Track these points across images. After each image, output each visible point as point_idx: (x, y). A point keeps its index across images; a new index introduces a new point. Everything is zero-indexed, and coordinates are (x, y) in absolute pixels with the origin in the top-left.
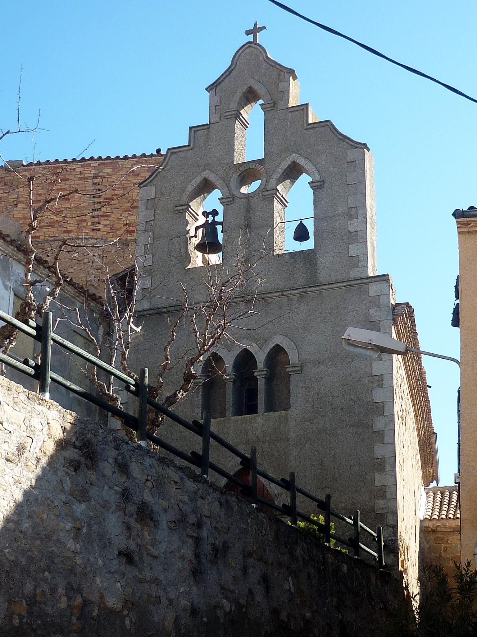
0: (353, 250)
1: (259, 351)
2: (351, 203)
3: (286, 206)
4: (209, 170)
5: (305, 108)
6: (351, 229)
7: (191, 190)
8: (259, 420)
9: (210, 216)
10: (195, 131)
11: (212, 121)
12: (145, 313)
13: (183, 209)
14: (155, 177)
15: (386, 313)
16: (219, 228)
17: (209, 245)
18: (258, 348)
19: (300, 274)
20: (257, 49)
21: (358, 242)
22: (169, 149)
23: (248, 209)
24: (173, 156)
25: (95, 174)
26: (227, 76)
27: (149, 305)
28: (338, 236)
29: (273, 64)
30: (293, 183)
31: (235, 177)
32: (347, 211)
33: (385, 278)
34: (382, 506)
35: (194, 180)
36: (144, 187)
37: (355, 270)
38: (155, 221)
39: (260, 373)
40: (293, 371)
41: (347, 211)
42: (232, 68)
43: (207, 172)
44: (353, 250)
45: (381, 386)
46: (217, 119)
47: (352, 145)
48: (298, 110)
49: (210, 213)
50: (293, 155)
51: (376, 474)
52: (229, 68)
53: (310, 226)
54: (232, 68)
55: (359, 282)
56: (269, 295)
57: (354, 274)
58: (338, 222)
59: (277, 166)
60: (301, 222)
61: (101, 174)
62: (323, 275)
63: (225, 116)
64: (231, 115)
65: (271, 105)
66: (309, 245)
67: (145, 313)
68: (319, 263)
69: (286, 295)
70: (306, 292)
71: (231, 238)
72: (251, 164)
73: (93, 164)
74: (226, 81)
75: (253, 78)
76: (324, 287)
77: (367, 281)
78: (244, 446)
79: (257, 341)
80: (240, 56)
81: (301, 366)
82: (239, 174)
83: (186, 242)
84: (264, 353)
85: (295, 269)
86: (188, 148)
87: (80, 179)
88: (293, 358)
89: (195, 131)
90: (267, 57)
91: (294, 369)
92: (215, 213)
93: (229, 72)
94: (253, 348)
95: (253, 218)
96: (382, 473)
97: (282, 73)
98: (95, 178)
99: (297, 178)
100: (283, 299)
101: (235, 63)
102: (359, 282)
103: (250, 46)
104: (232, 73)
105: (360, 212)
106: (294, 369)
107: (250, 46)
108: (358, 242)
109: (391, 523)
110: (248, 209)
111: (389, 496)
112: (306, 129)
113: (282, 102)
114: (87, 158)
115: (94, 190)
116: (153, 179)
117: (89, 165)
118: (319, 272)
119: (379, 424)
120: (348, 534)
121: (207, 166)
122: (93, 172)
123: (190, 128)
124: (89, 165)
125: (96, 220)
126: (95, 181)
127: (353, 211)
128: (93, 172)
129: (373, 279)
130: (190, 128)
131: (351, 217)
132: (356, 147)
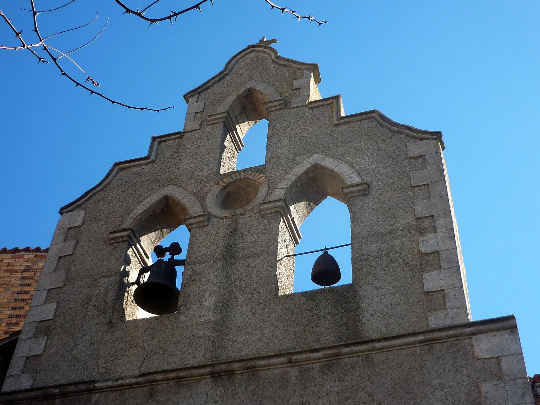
0: (432, 281)
2: (421, 210)
3: (297, 243)
5: (335, 104)
6: (424, 250)
7: (140, 211)
9: (167, 254)
10: (160, 142)
11: (187, 130)
12: (21, 396)
14: (88, 200)
16: (180, 269)
19: (326, 326)
21: (440, 268)
22: (117, 164)
24: (122, 173)
25: (28, 266)
26: (217, 82)
27: (31, 381)
28: (400, 261)
29: (285, 63)
30: (310, 209)
32: (414, 223)
33: (506, 325)
35: (148, 199)
37: (440, 314)
38: (74, 256)
41: (414, 223)
44: (432, 281)
46: (196, 125)
48: (323, 105)
49: (167, 249)
50: (314, 156)
52: (222, 72)
56: (262, 362)
57: (437, 320)
58: (399, 241)
60: (326, 252)
61: (35, 267)
62: (373, 324)
63: (209, 121)
64: (218, 119)
65: (281, 102)
67: (21, 396)
68: (363, 305)
69: (297, 361)
70: (338, 355)
71: (200, 274)
73: (27, 255)
74: (215, 87)
76: (378, 345)
77: (468, 330)
82: (222, 187)
83: (123, 287)
85: (315, 317)
86: (145, 161)
87: (6, 271)
90: (278, 57)
98: (25, 271)
99: (317, 203)
100: (289, 369)
102: (452, 332)
104: (224, 79)
105: (440, 223)
107: (253, 51)
108: (440, 268)
112: (336, 125)
114: (21, 247)
115: (21, 285)
116: (85, 202)
117: (22, 257)
118: (364, 320)
121: (171, 181)
122: (25, 264)
124: (22, 257)
125: (14, 320)
126: (25, 274)
127: (427, 223)
128: (25, 264)
131: (422, 231)
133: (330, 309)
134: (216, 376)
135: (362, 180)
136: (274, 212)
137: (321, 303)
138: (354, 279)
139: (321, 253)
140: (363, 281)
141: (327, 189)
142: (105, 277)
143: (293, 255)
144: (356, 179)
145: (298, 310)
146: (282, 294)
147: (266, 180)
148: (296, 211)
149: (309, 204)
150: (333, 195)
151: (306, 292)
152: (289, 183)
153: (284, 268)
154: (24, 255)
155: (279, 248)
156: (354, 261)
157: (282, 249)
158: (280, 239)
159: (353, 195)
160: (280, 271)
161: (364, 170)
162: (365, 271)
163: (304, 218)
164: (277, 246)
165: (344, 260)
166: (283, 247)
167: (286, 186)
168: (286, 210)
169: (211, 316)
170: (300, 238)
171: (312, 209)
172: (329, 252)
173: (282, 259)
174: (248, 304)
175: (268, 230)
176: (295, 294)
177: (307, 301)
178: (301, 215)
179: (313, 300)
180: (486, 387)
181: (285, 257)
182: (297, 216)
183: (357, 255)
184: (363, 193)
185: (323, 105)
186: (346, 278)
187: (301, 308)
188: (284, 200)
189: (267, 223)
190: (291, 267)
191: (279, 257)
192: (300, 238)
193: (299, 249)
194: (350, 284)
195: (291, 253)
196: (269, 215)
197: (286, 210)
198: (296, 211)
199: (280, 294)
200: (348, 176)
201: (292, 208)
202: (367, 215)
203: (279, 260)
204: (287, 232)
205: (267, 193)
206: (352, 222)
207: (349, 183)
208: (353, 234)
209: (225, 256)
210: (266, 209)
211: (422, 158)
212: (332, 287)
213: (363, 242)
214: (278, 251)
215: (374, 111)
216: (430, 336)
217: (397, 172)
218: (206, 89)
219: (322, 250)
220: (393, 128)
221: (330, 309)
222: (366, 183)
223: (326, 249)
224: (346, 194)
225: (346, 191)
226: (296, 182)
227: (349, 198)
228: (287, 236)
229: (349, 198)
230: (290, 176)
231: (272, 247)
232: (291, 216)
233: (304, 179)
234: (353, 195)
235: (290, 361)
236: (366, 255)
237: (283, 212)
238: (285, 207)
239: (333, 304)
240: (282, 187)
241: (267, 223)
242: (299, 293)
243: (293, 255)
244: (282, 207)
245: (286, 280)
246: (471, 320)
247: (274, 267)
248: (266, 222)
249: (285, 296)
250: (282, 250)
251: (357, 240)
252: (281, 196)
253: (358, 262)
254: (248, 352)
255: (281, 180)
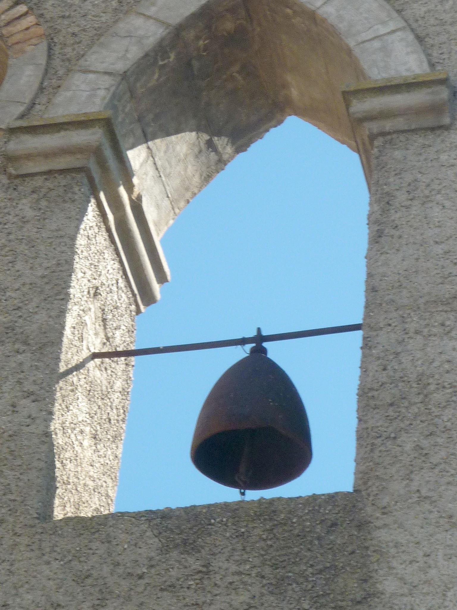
3: (148, 297)
60: (259, 352)
68: (389, 585)
99: (243, 136)
133: (256, 590)
135: (432, 65)
136: (62, 172)
137: (219, 563)
138: (364, 475)
139: (240, 353)
140: (397, 487)
141: (285, 86)
143: (128, 354)
144: (408, 61)
145: (125, 584)
146: (70, 511)
147: (40, 30)
148: (156, 168)
149: (210, 144)
150: (311, 113)
151: (165, 515)
152: (135, 53)
153: (83, 404)
154: (204, 42)
155: (70, 321)
156: (367, 397)
157: (83, 324)
158: (79, 286)
159: (388, 125)
160: (69, 417)
161: (442, 23)
162: (408, 447)
163: (183, 197)
164: (62, 313)
165: (328, 387)
166: (88, 319)
167: (120, 66)
168: (112, 163)
170: (162, 278)
171: (221, 163)
172: (275, 351)
173: (78, 367)
175: (31, 243)
176: (119, 517)
177: (165, 550)
178: (175, 183)
179: (189, 547)
181: (95, 356)
182: (157, 189)
183: (383, 377)
184: (429, 121)
186: (331, 467)
187: (141, 577)
188: (108, 125)
189: (29, 213)
190: (116, 397)
191: (69, 357)
192: (162, 278)
193: (162, 324)
194: (346, 495)
195: (120, 342)
196: (39, 181)
197: (112, 163)
198: (156, 168)
199: (58, 514)
200: (376, 44)
201: (136, 156)
202: (436, 212)
203: (69, 372)
204: (109, 254)
205: (41, 89)
206: (377, 237)
207: (377, 74)
208: (372, 290)
210: (29, 157)
212: (272, 502)
213: (412, 327)
214: (68, 332)
219: (243, 342)
221: (256, 590)
222: (444, 82)
223: (260, 339)
224: (361, 120)
225: (360, 106)
226: (161, 49)
227: (372, 137)
228: (110, 268)
229: (372, 137)
230: (139, 22)
231: (42, 317)
232: (130, 188)
233: (198, 38)
234: (388, 125)
236: (419, 381)
237: (99, 171)
238: (108, 153)
239: (267, 570)
240: (101, 67)
241: (29, 213)
242: (138, 516)
243: (128, 354)
244: (97, 152)
245: (89, 453)
247: (42, 399)
248: (26, 207)
249: (79, 525)
250: (82, 331)
251: (387, 315)
252: (96, 107)
253: (381, 403)
255: (100, 34)
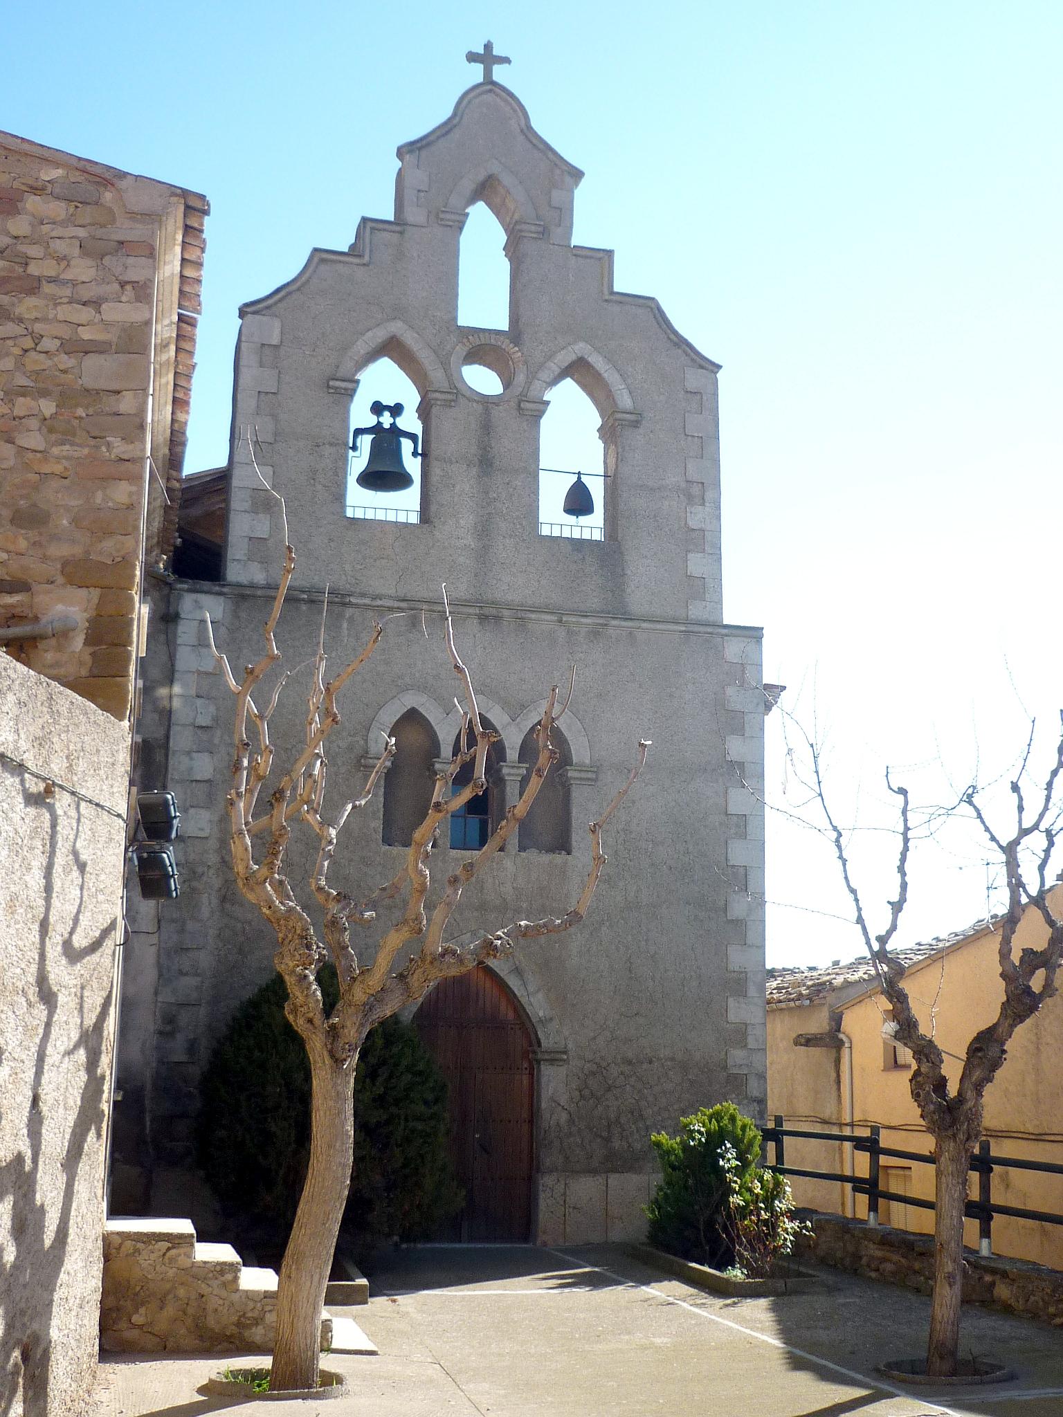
0: (696, 564)
1: (509, 724)
4: (403, 321)
7: (362, 352)
8: (508, 863)
13: (346, 389)
15: (755, 701)
16: (407, 446)
17: (384, 476)
18: (506, 718)
20: (506, 101)
21: (704, 551)
23: (487, 427)
24: (323, 267)
26: (443, 135)
29: (541, 146)
31: (461, 350)
33: (754, 634)
34: (739, 1062)
36: (254, 313)
39: (512, 771)
40: (581, 779)
41: (683, 485)
42: (455, 122)
43: (400, 324)
45: (743, 836)
47: (693, 360)
48: (591, 257)
49: (388, 408)
50: (582, 344)
51: (731, 1000)
53: (597, 489)
54: (455, 122)
55: (709, 630)
59: (550, 357)
60: (579, 478)
64: (454, 221)
66: (592, 526)
67: (259, 593)
68: (629, 572)
72: (493, 336)
75: (487, 154)
76: (645, 625)
78: (475, 914)
79: (505, 704)
80: (469, 102)
81: (595, 770)
84: (521, 730)
88: (580, 752)
89: (372, 229)
90: (530, 128)
91: (583, 775)
92: (397, 410)
93: (446, 129)
94: (498, 717)
95: (495, 448)
96: (741, 999)
97: (558, 172)
101: (459, 113)
103: (490, 91)
105: (709, 495)
106: (583, 775)
107: (490, 91)
108: (704, 551)
109: (756, 1093)
110: (487, 427)
111: (752, 1043)
113: (559, 230)
116: (276, 303)
118: (629, 590)
119: (738, 909)
120: (676, 1107)
121: (398, 312)
123: (365, 220)
127: (696, 490)
129: (734, 632)
130: (365, 220)
132: (702, 367)
134: (483, 618)
142: (331, 444)
169: (470, 541)
174: (511, 536)
179: (579, 551)
180: (730, 691)
185: (591, 257)
209: (481, 462)
211: (699, 397)
215: (653, 299)
216: (691, 628)
217: (662, 393)
218: (428, 144)
220: (672, 336)
235: (560, 621)
246: (725, 622)
254: (514, 597)
